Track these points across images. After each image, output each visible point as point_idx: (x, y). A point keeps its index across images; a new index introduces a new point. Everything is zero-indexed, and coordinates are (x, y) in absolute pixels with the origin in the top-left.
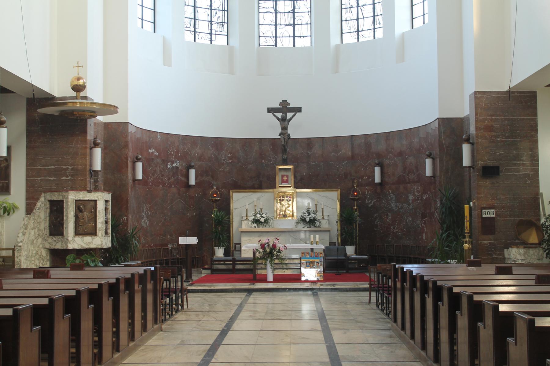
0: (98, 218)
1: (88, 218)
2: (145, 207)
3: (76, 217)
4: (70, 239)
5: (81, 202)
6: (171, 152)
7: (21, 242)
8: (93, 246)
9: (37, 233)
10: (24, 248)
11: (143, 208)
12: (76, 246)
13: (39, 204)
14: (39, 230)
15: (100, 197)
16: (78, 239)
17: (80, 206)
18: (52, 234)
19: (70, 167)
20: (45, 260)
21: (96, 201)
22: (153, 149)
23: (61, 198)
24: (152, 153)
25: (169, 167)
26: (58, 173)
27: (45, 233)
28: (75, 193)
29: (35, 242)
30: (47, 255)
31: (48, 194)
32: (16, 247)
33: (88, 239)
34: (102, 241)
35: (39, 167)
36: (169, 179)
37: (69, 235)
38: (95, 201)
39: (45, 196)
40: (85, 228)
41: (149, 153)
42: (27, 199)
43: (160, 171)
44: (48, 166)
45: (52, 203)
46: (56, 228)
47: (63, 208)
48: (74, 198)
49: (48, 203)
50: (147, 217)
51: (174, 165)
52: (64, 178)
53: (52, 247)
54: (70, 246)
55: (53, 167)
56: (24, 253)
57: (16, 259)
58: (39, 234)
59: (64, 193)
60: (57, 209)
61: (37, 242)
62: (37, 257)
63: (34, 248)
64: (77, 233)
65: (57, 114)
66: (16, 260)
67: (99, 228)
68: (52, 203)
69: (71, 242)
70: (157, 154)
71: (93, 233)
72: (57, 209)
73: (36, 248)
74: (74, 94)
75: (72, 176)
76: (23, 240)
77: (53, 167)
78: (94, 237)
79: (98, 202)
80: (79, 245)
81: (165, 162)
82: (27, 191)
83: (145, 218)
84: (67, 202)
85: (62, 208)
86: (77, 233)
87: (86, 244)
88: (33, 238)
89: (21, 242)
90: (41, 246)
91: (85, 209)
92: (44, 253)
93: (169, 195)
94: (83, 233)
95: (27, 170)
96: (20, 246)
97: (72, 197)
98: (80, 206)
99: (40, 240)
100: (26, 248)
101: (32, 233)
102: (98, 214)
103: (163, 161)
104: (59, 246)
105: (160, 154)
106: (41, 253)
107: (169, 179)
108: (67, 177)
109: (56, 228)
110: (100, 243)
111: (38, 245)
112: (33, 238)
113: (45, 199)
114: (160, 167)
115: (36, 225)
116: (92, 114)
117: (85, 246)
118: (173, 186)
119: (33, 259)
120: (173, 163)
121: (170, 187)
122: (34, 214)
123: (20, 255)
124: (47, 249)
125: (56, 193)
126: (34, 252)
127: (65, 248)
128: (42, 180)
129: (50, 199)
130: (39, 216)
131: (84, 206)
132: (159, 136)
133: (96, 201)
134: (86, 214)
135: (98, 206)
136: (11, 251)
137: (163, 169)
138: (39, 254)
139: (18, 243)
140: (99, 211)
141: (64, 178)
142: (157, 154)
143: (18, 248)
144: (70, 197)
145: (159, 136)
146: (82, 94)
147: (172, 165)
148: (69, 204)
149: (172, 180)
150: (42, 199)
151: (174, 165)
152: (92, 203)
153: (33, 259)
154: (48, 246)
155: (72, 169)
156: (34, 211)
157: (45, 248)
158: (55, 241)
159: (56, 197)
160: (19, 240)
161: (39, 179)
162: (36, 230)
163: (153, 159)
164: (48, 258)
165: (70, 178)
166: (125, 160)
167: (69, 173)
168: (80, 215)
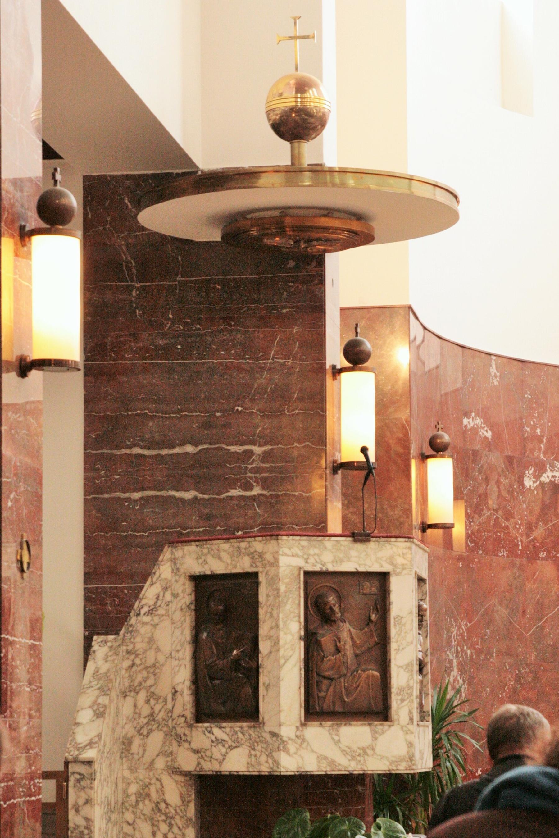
0: (393, 646)
1: (354, 645)
2: (455, 631)
3: (310, 640)
4: (287, 732)
5: (327, 582)
6: (534, 428)
7: (91, 744)
8: (376, 765)
9: (146, 711)
10: (101, 770)
11: (449, 632)
12: (311, 765)
13: (150, 592)
14: (152, 696)
15: (400, 560)
16: (319, 734)
17: (323, 596)
18: (205, 711)
19: (258, 450)
20: (178, 820)
21: (384, 577)
22: (477, 414)
23: (244, 565)
24: (475, 430)
25: (528, 482)
26: (204, 471)
27: (178, 710)
28: (304, 542)
29: (135, 747)
30: (185, 803)
31: (192, 548)
32: (72, 768)
33: (356, 733)
34: (410, 745)
35: (137, 451)
36: (530, 528)
37: (283, 718)
38: (383, 577)
39: (174, 561)
40: (346, 692)
41: (464, 432)
42: (88, 577)
43: (500, 496)
44: (172, 447)
45: (204, 586)
46: (226, 687)
47: (254, 604)
48: (300, 562)
49: (189, 587)
50: (462, 669)
51: (545, 478)
52: (234, 492)
53: (209, 767)
54: (289, 764)
55: (190, 449)
56: (102, 791)
57: (71, 814)
58: (152, 716)
59: (258, 545)
60: (226, 609)
61: (144, 746)
62: (147, 807)
63: (133, 769)
64: (314, 711)
65: (216, 236)
66: (74, 819)
67: (401, 690)
68: (204, 586)
69: (292, 747)
70: (489, 434)
71: (378, 710)
72: (226, 609)
73: (142, 774)
74: (279, 152)
75: (265, 484)
76: (99, 736)
77: (190, 449)
78: (379, 726)
79: (394, 583)
80: (321, 758)
81: (515, 464)
82: (90, 546)
83: (455, 673)
84: (274, 580)
85: (253, 604)
86: (314, 711)
87: (348, 752)
88: (129, 730)
89: (91, 744)
90: (160, 763)
91: (344, 608)
92: (174, 792)
93: (529, 586)
94: (339, 708)
95: (90, 462)
96: (89, 763)
97: (288, 561)
98: (323, 596)
99: (156, 739)
100: (106, 771)
101: (127, 708)
102: (393, 631)
103: (510, 460)
104: (237, 762)
105: (497, 435)
106: (161, 791)
107: (530, 528)
108: (248, 487)
109: (226, 687)
110: (402, 751)
111: (147, 759)
112: (129, 730)
113: (176, 571)
114: (498, 482)
115: (139, 678)
116: (355, 226)
117: (346, 765)
118: (543, 555)
119: (129, 817)
120: (541, 468)
121: (533, 557)
122: (132, 632)
123: (87, 802)
124: (187, 774)
125: (225, 546)
126: (133, 789)
127: (265, 769)
128: (147, 500)
129: (197, 569)
130: (151, 640)
131: (340, 599)
132: (493, 370)
133: (384, 577)
134: (348, 634)
135: (394, 597)
136: (52, 784)
137: (511, 492)
138: (154, 795)
139: (81, 749)
140: (399, 618)
141: (234, 492)
142: (489, 434)
143: (82, 769)
144: (284, 561)
145: (493, 370)
146: (309, 152)
147: (537, 477)
148: (283, 588)
149: (539, 532)
150: (164, 571)
151: (545, 478)
152: (371, 587)
153: (129, 817)
154: (188, 762)
155: (266, 457)
156: (133, 620)
157: (175, 771)
158: (218, 741)
159: (221, 559)
160: (81, 738)
161: (136, 495)
162: (142, 696)
163: (475, 453)
164: (191, 811)
165: (257, 491)
166: (400, 449)
167: (255, 471)
168: (326, 640)
